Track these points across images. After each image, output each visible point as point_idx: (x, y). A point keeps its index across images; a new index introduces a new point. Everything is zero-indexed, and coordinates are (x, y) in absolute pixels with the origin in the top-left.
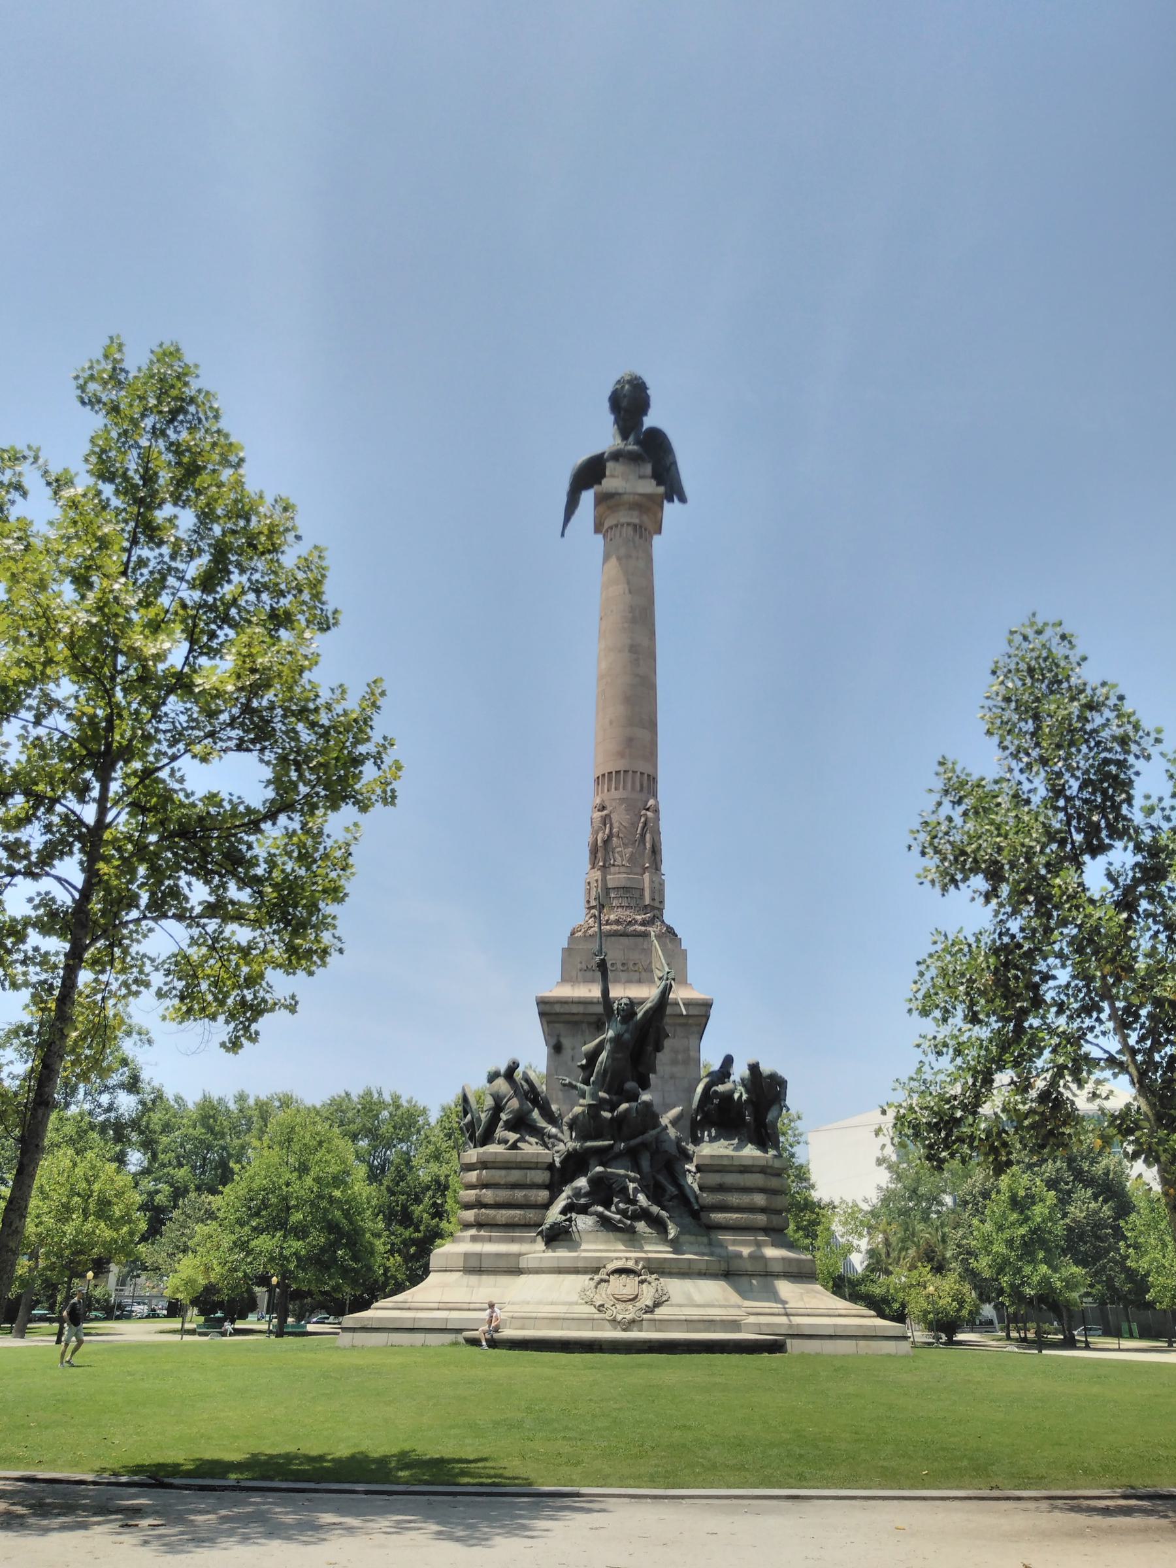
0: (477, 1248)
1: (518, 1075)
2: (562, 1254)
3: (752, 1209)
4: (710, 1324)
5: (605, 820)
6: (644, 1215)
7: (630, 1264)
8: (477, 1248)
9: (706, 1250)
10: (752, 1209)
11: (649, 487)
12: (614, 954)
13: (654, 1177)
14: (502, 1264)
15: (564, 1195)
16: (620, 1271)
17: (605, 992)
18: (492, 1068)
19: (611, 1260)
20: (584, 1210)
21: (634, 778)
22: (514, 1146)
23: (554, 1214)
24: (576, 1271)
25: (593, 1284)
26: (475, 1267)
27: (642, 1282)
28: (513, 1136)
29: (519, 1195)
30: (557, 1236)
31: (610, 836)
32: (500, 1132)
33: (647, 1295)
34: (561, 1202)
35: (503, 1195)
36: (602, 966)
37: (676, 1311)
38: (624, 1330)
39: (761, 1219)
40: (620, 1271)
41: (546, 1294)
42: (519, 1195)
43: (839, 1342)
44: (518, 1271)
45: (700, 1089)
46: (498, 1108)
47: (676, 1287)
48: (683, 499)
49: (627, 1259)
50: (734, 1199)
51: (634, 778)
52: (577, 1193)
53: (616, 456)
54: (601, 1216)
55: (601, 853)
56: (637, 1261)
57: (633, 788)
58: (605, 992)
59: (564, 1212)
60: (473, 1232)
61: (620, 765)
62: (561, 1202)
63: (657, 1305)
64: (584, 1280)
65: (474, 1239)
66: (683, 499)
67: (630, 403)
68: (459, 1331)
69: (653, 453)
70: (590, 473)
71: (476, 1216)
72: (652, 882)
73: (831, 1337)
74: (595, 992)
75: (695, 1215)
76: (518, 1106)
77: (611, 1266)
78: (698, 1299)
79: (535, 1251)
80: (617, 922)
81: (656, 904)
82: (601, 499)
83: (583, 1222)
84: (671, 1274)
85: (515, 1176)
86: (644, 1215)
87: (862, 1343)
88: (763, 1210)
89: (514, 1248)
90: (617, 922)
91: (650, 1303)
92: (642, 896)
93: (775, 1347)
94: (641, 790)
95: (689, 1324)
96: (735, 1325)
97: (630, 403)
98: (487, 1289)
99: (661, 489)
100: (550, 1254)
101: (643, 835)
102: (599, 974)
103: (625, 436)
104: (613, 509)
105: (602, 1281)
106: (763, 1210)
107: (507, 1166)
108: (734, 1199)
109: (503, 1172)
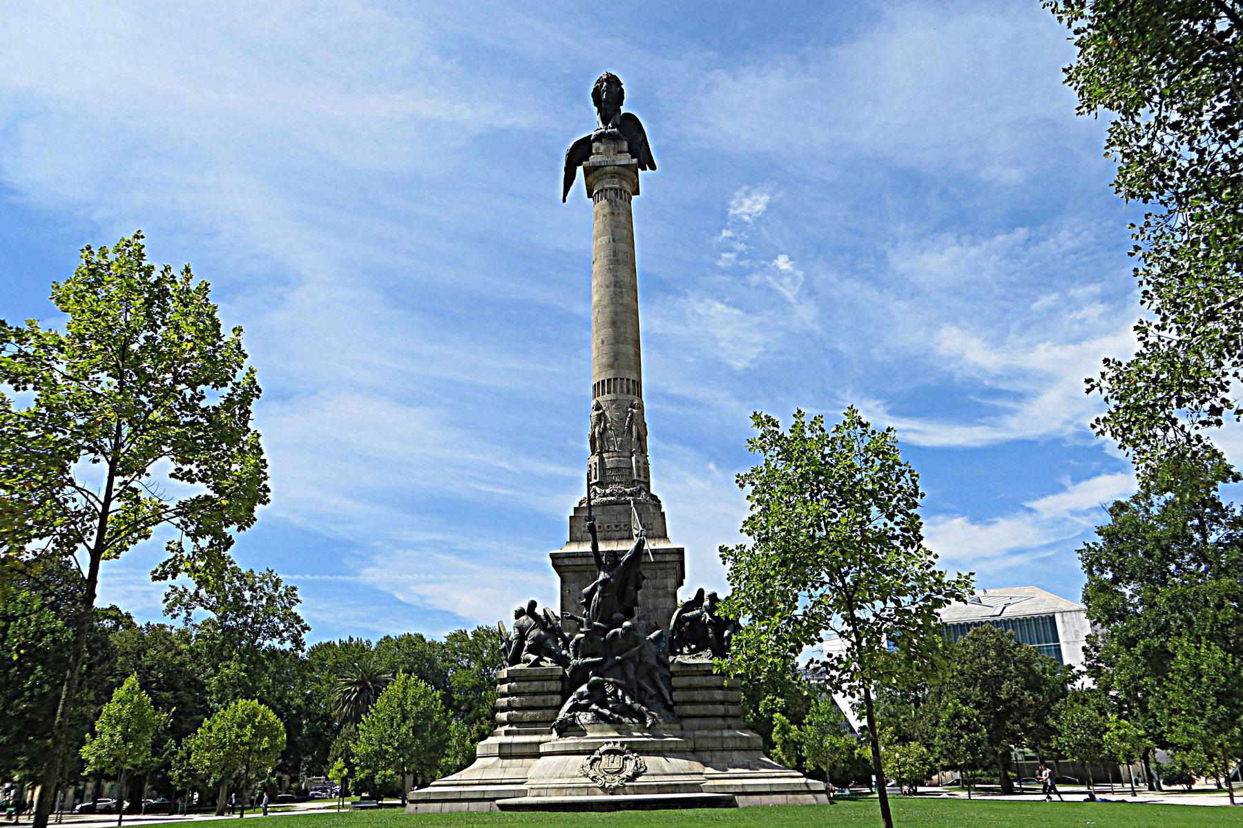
0: (509, 739)
1: (539, 611)
2: (571, 741)
3: (713, 702)
4: (676, 788)
5: (600, 418)
6: (629, 711)
7: (618, 746)
8: (509, 739)
9: (680, 733)
10: (713, 702)
11: (626, 159)
12: (600, 519)
13: (638, 683)
14: (527, 750)
15: (571, 699)
16: (608, 752)
17: (595, 547)
18: (517, 608)
19: (602, 744)
20: (585, 708)
21: (623, 380)
22: (536, 664)
23: (563, 714)
24: (578, 753)
26: (506, 753)
27: (626, 759)
28: (533, 657)
29: (539, 700)
30: (565, 729)
31: (605, 429)
32: (525, 655)
33: (630, 769)
34: (568, 705)
36: (592, 529)
37: (652, 778)
38: (612, 794)
39: (721, 709)
40: (608, 752)
41: (555, 772)
42: (539, 700)
43: (774, 796)
44: (538, 755)
45: (674, 616)
46: (522, 636)
47: (651, 762)
48: (653, 167)
49: (615, 743)
50: (698, 695)
51: (623, 380)
52: (581, 697)
53: (599, 138)
54: (596, 711)
55: (598, 443)
56: (622, 744)
57: (622, 392)
58: (595, 547)
59: (569, 711)
60: (507, 728)
61: (609, 375)
62: (568, 705)
63: (637, 774)
64: (583, 759)
65: (507, 733)
66: (653, 167)
67: (608, 96)
68: (493, 799)
69: (628, 134)
70: (580, 152)
71: (508, 716)
72: (637, 462)
73: (767, 793)
74: (587, 548)
75: (669, 709)
76: (541, 633)
77: (605, 747)
78: (668, 770)
79: (553, 741)
80: (611, 494)
81: (642, 479)
82: (587, 173)
83: (584, 718)
84: (648, 753)
85: (535, 686)
86: (629, 711)
87: (790, 796)
88: (722, 703)
89: (536, 738)
90: (611, 494)
91: (630, 774)
92: (631, 473)
93: (729, 803)
94: (628, 392)
95: (660, 788)
96: (696, 787)
97: (608, 96)
98: (514, 768)
99: (635, 161)
100: (562, 741)
101: (630, 427)
102: (590, 535)
103: (605, 121)
104: (600, 178)
105: (596, 760)
106: (722, 703)
107: (529, 678)
108: (698, 695)
109: (527, 684)
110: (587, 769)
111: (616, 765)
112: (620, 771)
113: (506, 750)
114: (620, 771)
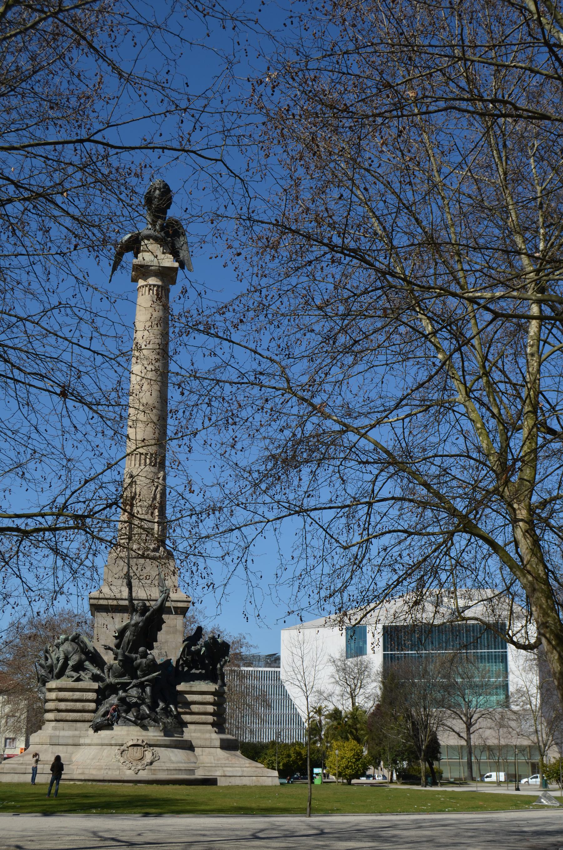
14: (70, 741)
25: (119, 752)
28: (75, 675)
29: (79, 705)
32: (68, 672)
33: (148, 756)
35: (70, 705)
42: (79, 705)
91: (149, 761)
109: (71, 693)
110: (119, 757)
111: (138, 755)
112: (141, 759)
113: (55, 741)
114: (141, 759)
